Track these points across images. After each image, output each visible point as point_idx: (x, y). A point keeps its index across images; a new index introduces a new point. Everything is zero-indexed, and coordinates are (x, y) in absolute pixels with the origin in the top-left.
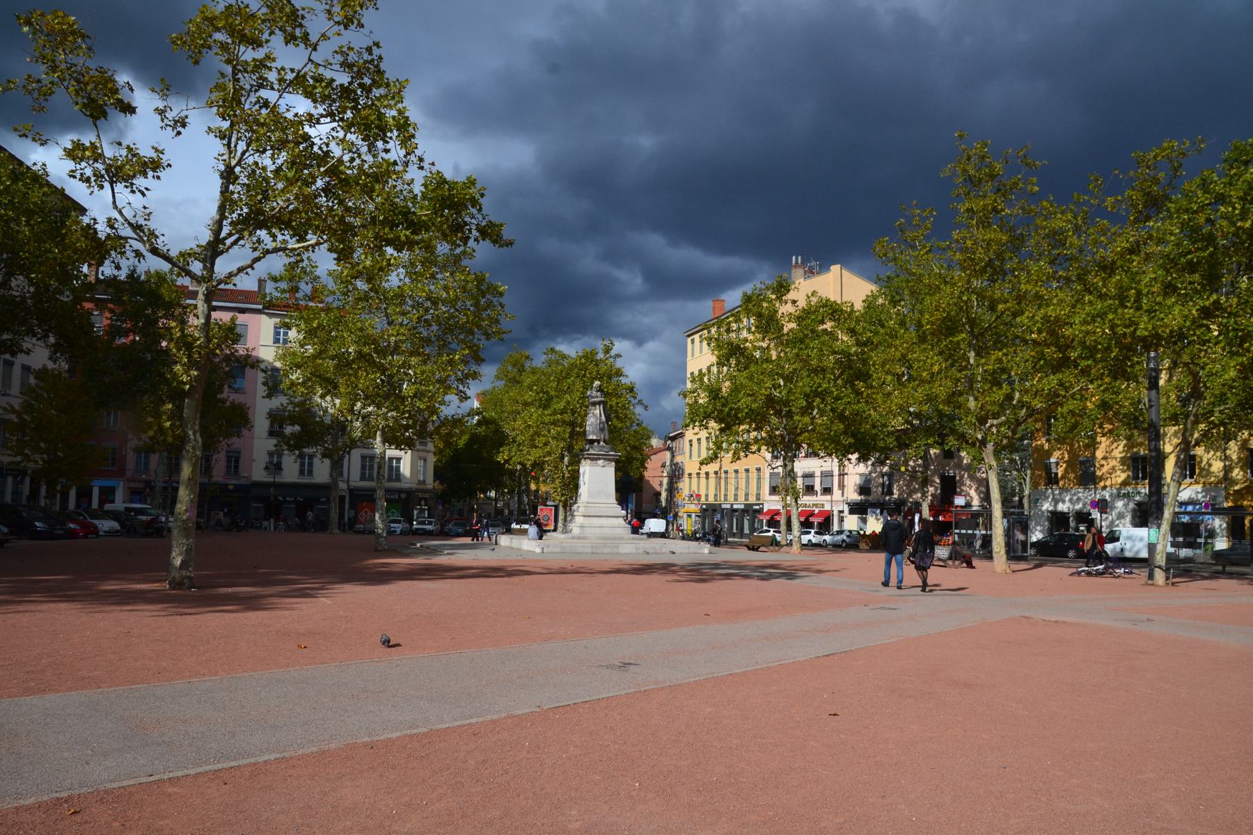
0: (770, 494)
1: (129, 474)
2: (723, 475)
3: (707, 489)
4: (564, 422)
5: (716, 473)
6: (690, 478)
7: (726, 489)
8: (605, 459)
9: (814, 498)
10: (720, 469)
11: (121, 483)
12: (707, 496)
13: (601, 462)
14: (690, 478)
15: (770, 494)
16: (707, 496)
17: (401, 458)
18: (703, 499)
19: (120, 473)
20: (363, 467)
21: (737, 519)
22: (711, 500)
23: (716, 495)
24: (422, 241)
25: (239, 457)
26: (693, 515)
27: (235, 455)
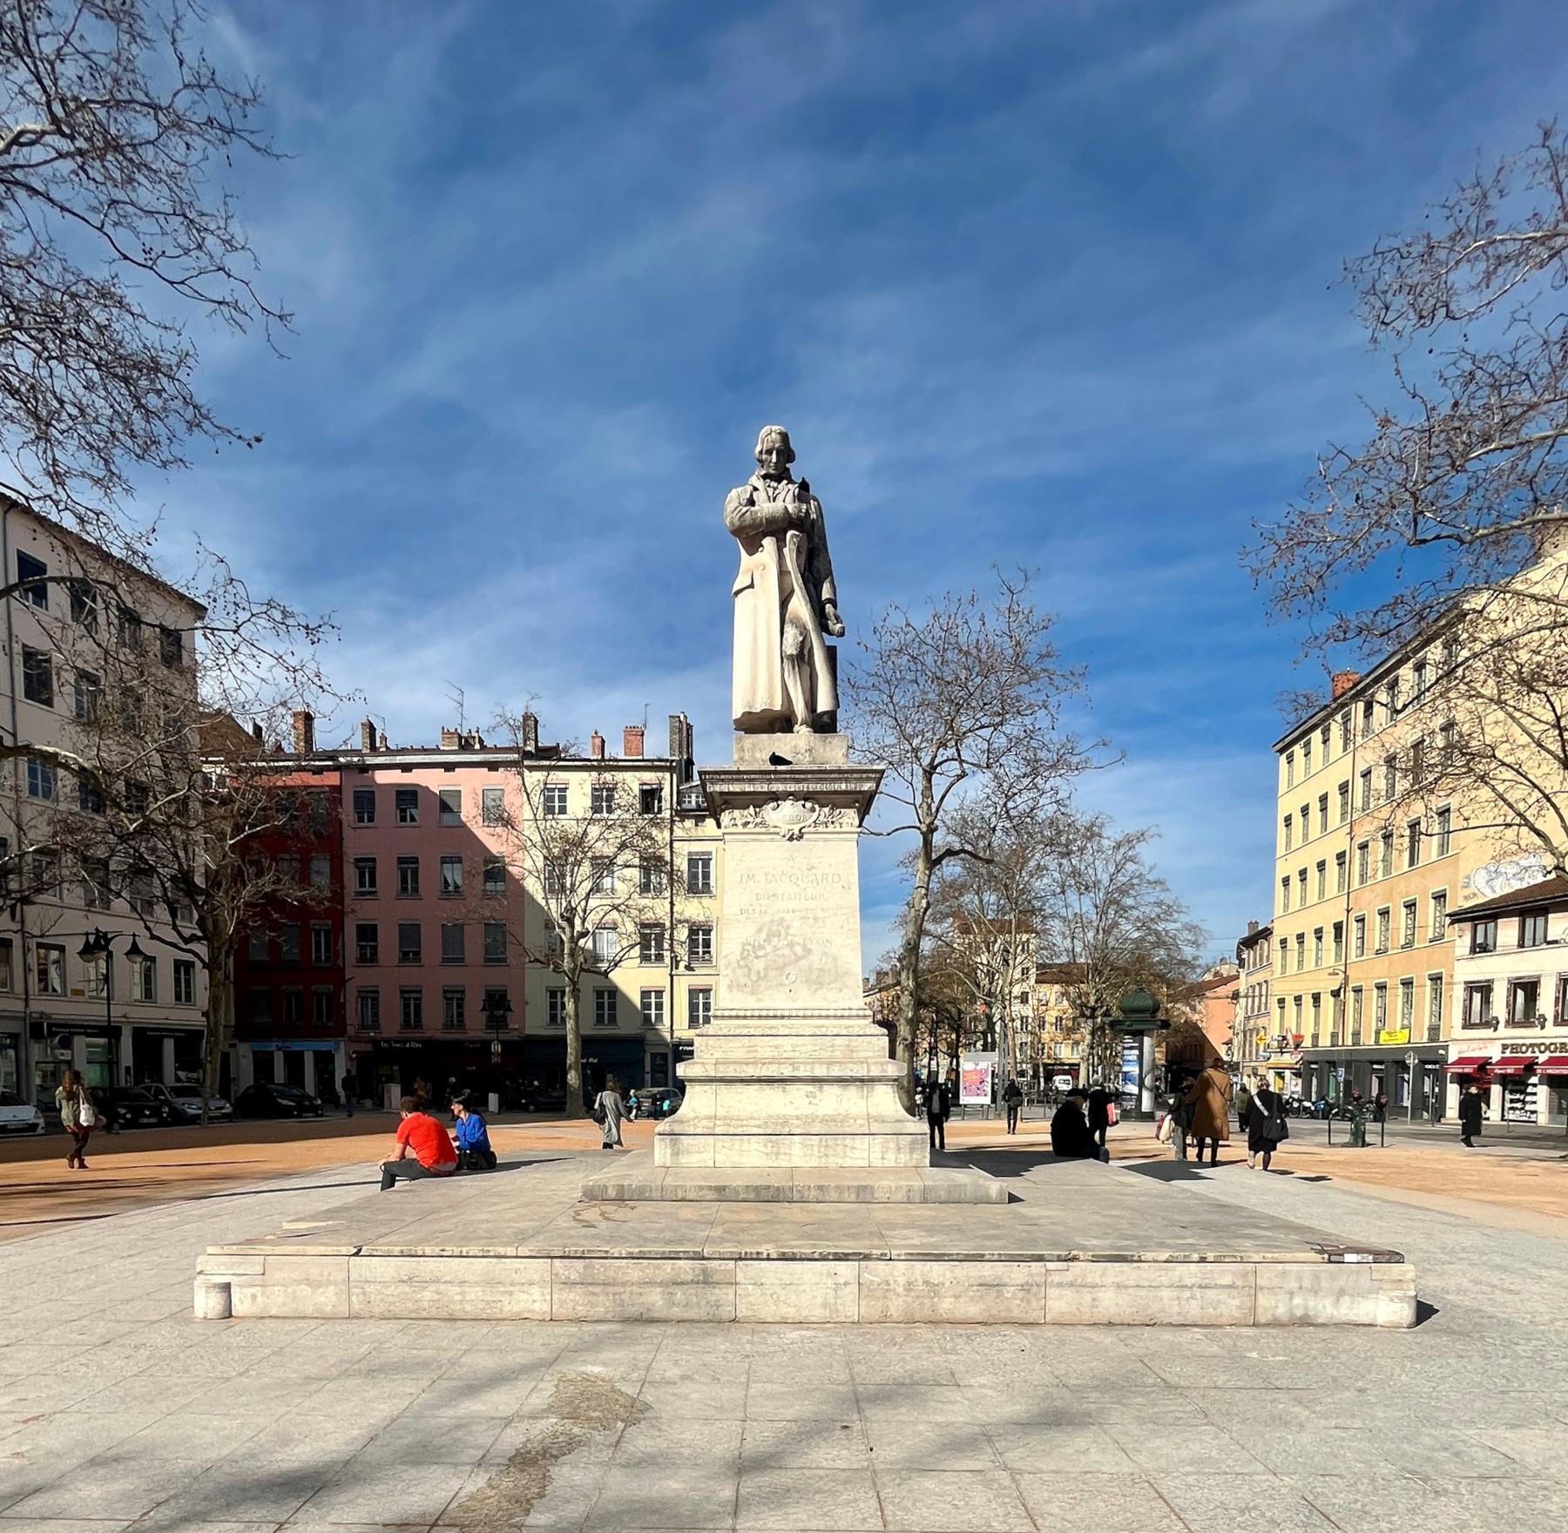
0: (359, 927)
1: (351, 1031)
2: (1351, 995)
3: (1317, 1023)
4: (125, 157)
5: (1335, 994)
6: (1299, 1005)
7: (1358, 1021)
8: (806, 797)
9: (1536, 1031)
10: (1346, 984)
11: (342, 1045)
12: (1315, 1037)
13: (784, 814)
14: (1299, 1005)
15: (359, 927)
16: (1315, 1037)
17: (710, 990)
18: (1307, 1043)
19: (339, 1030)
20: (600, 1006)
21: (1381, 1080)
22: (1325, 1042)
23: (1334, 1035)
24: (1509, 1472)
25: (463, 999)
26: (1287, 1073)
27: (373, 995)
